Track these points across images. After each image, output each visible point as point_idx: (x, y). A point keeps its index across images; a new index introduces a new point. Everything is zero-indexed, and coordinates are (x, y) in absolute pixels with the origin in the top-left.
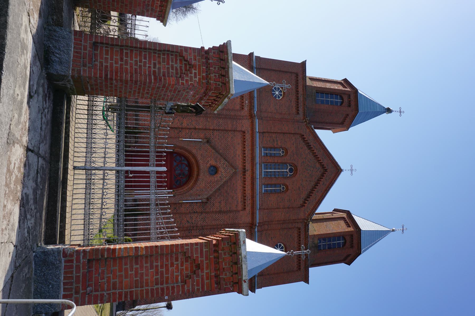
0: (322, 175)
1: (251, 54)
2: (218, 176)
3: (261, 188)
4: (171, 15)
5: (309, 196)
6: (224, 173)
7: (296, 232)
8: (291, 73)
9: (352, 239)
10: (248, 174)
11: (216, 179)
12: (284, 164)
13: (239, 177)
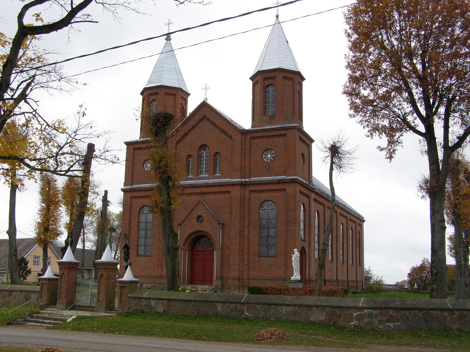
0: (208, 119)
1: (122, 190)
2: (204, 216)
3: (219, 177)
4: (358, 118)
5: (224, 132)
6: (200, 211)
7: (254, 141)
8: (134, 154)
9: (267, 78)
10: (205, 190)
11: (206, 217)
12: (200, 156)
13: (207, 197)
